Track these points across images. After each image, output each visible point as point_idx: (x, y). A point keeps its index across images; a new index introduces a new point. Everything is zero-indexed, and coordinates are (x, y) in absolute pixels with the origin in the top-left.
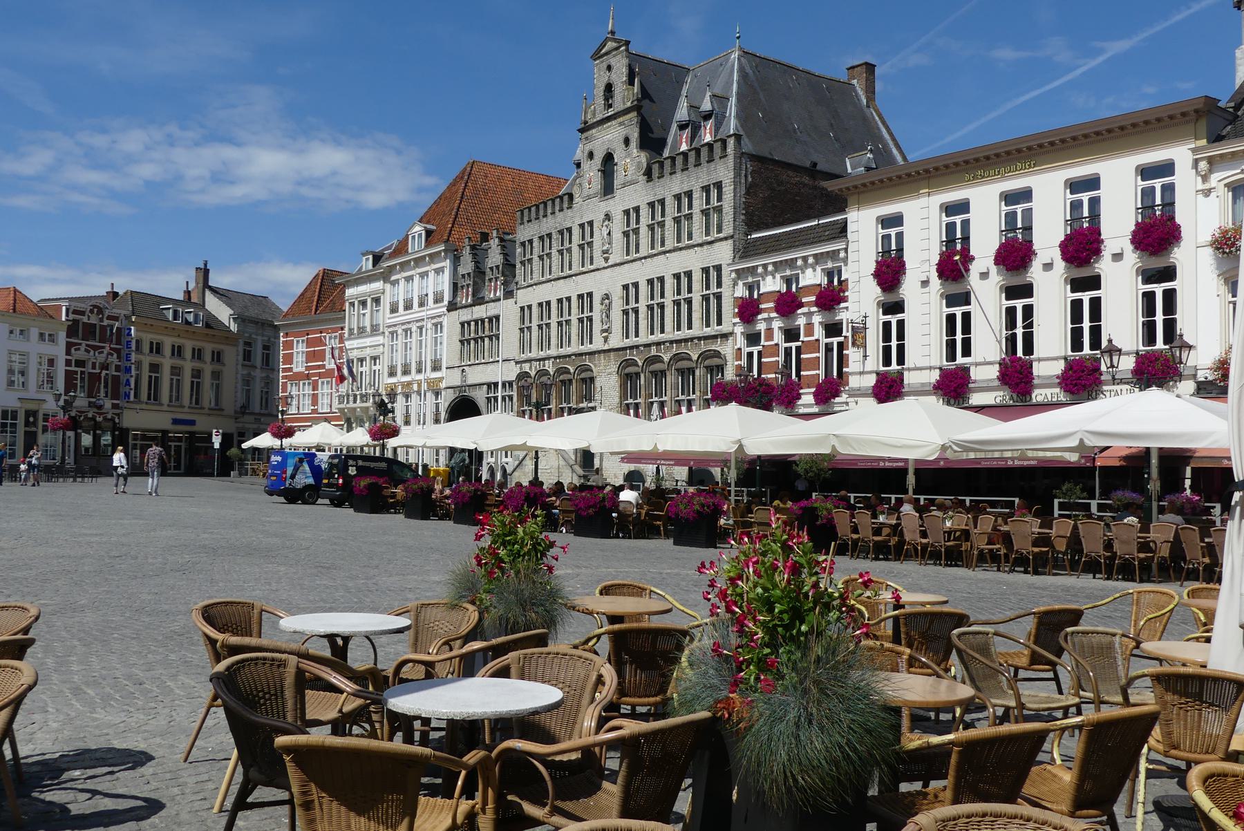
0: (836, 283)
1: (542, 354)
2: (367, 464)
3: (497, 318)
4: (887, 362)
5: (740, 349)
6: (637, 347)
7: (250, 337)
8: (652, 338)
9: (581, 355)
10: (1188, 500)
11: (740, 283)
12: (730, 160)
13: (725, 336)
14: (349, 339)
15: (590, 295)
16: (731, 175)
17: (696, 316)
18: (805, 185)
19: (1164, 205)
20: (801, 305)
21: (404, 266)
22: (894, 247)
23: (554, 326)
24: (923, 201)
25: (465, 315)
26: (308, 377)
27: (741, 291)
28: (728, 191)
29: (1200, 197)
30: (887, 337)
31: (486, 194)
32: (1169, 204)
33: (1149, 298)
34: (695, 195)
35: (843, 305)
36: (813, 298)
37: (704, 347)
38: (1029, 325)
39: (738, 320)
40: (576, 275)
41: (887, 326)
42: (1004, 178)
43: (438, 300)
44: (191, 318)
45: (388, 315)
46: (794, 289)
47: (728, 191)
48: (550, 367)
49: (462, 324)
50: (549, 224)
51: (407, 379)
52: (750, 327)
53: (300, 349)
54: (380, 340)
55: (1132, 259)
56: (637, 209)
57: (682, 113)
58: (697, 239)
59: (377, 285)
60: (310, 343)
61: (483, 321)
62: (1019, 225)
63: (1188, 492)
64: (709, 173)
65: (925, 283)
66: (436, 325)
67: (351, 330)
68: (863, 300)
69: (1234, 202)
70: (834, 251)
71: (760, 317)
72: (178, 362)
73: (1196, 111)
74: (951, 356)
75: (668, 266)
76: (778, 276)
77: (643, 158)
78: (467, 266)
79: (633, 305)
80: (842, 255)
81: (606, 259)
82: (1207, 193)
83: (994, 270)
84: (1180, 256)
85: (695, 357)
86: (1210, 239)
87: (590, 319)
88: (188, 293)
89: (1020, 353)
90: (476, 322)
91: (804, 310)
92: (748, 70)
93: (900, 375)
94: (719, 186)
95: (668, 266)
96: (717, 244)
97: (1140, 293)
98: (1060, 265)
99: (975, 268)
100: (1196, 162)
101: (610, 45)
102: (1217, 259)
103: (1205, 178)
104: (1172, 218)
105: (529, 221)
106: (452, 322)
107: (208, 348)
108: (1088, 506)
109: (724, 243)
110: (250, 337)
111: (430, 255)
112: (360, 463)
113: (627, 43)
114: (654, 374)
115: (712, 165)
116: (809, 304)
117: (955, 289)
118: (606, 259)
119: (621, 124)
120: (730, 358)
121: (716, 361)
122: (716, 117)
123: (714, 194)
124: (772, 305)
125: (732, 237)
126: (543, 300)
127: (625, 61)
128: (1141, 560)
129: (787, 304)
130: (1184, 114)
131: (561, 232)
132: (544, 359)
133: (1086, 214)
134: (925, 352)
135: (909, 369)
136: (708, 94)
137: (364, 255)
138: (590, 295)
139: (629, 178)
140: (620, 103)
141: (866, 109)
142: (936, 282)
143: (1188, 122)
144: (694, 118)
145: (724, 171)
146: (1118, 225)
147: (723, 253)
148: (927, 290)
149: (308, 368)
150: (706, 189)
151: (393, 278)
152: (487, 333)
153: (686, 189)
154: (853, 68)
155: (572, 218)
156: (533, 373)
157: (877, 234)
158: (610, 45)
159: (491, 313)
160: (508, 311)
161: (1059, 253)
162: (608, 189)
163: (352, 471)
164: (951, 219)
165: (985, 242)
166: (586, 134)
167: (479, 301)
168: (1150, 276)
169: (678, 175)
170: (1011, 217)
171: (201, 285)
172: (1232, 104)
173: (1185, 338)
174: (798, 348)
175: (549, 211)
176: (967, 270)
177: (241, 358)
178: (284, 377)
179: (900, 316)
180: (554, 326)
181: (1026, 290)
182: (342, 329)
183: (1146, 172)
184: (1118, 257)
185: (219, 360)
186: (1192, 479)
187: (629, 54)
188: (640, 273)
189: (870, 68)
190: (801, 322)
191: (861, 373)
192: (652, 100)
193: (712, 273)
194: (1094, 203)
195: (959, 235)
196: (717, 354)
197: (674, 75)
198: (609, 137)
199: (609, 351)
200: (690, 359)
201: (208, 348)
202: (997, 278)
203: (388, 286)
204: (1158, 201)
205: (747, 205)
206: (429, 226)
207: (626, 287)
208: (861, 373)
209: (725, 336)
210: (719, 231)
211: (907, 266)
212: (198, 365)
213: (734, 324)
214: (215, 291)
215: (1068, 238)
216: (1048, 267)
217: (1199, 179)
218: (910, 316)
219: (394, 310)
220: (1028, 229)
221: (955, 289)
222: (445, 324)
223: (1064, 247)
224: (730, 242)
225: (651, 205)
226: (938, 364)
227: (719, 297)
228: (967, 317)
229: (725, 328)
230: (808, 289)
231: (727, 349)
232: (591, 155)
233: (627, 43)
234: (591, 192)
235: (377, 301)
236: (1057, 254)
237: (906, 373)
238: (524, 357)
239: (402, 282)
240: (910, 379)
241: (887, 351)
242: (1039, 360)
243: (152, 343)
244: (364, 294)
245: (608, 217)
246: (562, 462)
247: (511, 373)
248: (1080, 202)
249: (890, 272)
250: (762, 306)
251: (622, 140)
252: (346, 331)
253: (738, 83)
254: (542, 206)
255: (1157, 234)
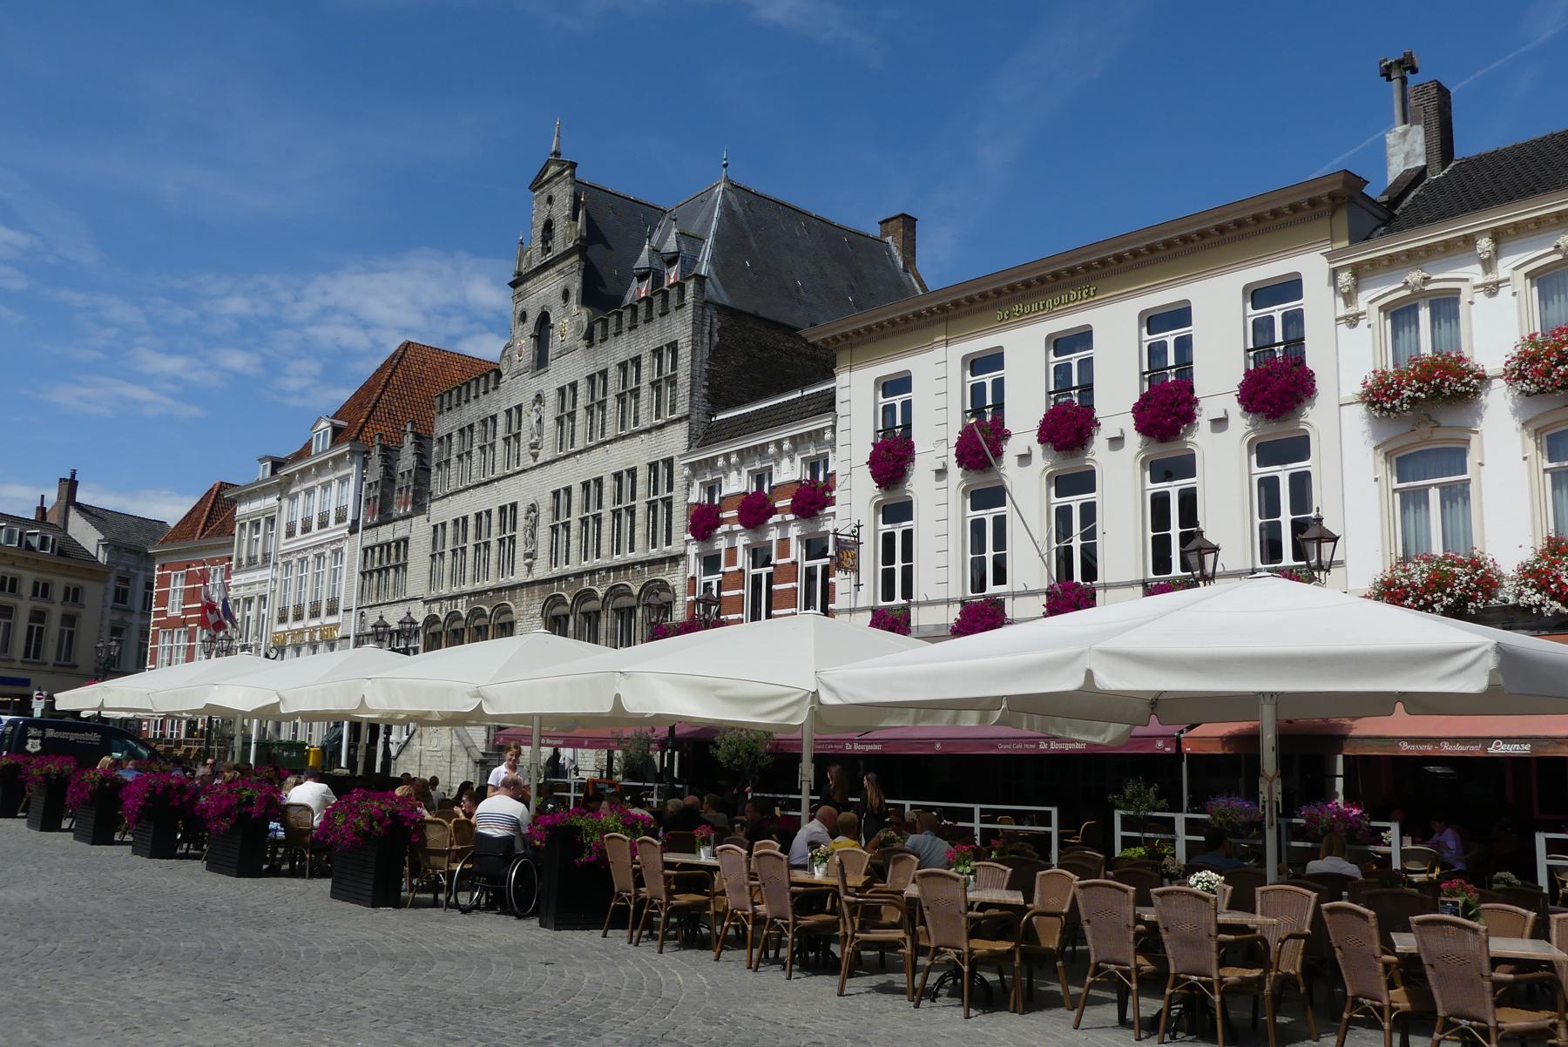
0: (821, 478)
1: (455, 590)
2: (63, 735)
3: (406, 540)
4: (888, 594)
5: (693, 578)
6: (565, 577)
7: (127, 571)
8: (586, 565)
9: (500, 590)
10: (1340, 813)
11: (697, 483)
12: (689, 311)
13: (674, 560)
14: (236, 573)
15: (514, 506)
16: (689, 331)
17: (640, 531)
18: (800, 354)
19: (1286, 342)
20: (775, 511)
21: (304, 473)
22: (899, 423)
23: (470, 550)
24: (939, 353)
25: (370, 538)
26: (184, 623)
27: (697, 495)
28: (685, 353)
29: (1343, 328)
30: (888, 557)
31: (421, 382)
32: (1295, 342)
33: (1269, 488)
34: (645, 362)
35: (828, 510)
36: (788, 502)
37: (647, 575)
38: (1089, 534)
39: (689, 536)
40: (498, 480)
41: (889, 539)
42: (1052, 314)
43: (340, 519)
44: (35, 542)
45: (283, 539)
46: (766, 490)
47: (685, 353)
48: (462, 608)
49: (365, 550)
50: (471, 412)
51: (298, 625)
52: (707, 546)
53: (178, 585)
54: (266, 574)
55: (1241, 425)
56: (574, 386)
57: (643, 260)
58: (645, 423)
59: (272, 501)
60: (189, 578)
61: (389, 545)
62: (1075, 383)
63: (1340, 800)
64: (661, 331)
65: (941, 473)
66: (335, 552)
67: (240, 560)
68: (855, 502)
69: (1395, 336)
70: (817, 431)
71: (719, 531)
72: (41, 605)
73: (1332, 196)
74: (979, 585)
75: (606, 463)
76: (745, 471)
77: (584, 316)
78: (375, 473)
79: (563, 519)
80: (828, 436)
81: (535, 456)
82: (1353, 321)
83: (1038, 449)
84: (1316, 418)
85: (636, 591)
86: (1360, 389)
87: (512, 539)
88: (42, 510)
89: (1077, 577)
90: (381, 546)
91: (776, 518)
92: (736, 206)
93: (906, 611)
94: (673, 347)
95: (606, 463)
96: (669, 429)
97: (1255, 479)
98: (1134, 440)
99: (1011, 450)
100: (1334, 273)
101: (553, 169)
102: (1374, 421)
103: (1349, 298)
104: (1300, 361)
105: (449, 409)
106: (353, 548)
107: (59, 584)
108: (1169, 825)
109: (677, 426)
110: (127, 571)
111: (335, 459)
112: (50, 733)
113: (573, 166)
114: (586, 614)
115: (667, 319)
116: (783, 510)
117: (982, 481)
118: (535, 456)
119: (560, 272)
120: (679, 591)
121: (664, 596)
122: (683, 262)
123: (668, 359)
124: (734, 513)
125: (687, 417)
126: (459, 515)
127: (569, 189)
128: (1230, 991)
129: (755, 511)
130: (1313, 203)
131: (484, 422)
132: (456, 597)
133: (1171, 361)
134: (940, 575)
135: (918, 604)
136: (674, 231)
137: (261, 460)
138: (514, 506)
139: (566, 345)
140: (559, 245)
141: (904, 276)
142: (955, 472)
143: (1319, 216)
144: (657, 264)
145: (679, 327)
146: (1219, 373)
147: (675, 441)
148: (943, 484)
149: (185, 611)
150: (657, 353)
151: (293, 491)
152: (393, 562)
153: (633, 355)
154: (887, 221)
155: (496, 403)
156: (442, 617)
157: (876, 404)
158: (553, 169)
159: (400, 534)
160: (418, 531)
161: (1133, 421)
162: (541, 362)
163: (33, 746)
164: (978, 379)
165: (1025, 410)
166: (519, 289)
167: (386, 518)
168: (1267, 452)
169: (625, 336)
170: (1062, 371)
171: (64, 501)
172: (1385, 198)
173: (1325, 524)
174: (769, 576)
175: (473, 394)
176: (998, 454)
177: (110, 598)
178: (156, 624)
179: (906, 525)
180: (470, 550)
181: (1084, 481)
182: (230, 559)
183: (1259, 295)
184: (1220, 424)
185: (75, 599)
186: (1345, 776)
187: (576, 183)
188: (572, 474)
189: (908, 222)
190: (774, 536)
191: (851, 611)
192: (608, 247)
193: (661, 469)
194: (1184, 345)
195: (989, 402)
196: (664, 586)
197: (646, 216)
198: (546, 290)
199: (533, 583)
200: (631, 595)
201: (59, 584)
202: (1042, 462)
203: (285, 502)
204: (1279, 338)
205: (711, 375)
206: (337, 422)
207: (556, 494)
208: (851, 611)
209: (674, 560)
210: (672, 412)
211: (917, 449)
212: (41, 605)
213: (687, 542)
214: (84, 510)
215: (1144, 397)
216: (1117, 442)
217: (1340, 301)
218: (921, 523)
219: (290, 534)
220: (1087, 389)
221: (982, 481)
222: (346, 550)
223: (1138, 410)
224: (685, 424)
225: (591, 378)
226: (959, 595)
227: (668, 503)
228: (1000, 522)
229: (675, 548)
230: (779, 490)
231: (676, 579)
232: (523, 317)
233: (573, 166)
234: (522, 365)
235: (271, 521)
236: (1129, 422)
237: (913, 610)
238: (434, 594)
239: (302, 496)
240: (919, 617)
241: (888, 576)
242: (1106, 587)
243: (67, 589)
244: (257, 513)
245: (539, 398)
246: (456, 742)
247: (420, 614)
248: (1163, 345)
249: (891, 460)
250: (724, 515)
251: (560, 292)
252: (234, 563)
253: (719, 221)
254: (464, 388)
255: (1278, 387)
